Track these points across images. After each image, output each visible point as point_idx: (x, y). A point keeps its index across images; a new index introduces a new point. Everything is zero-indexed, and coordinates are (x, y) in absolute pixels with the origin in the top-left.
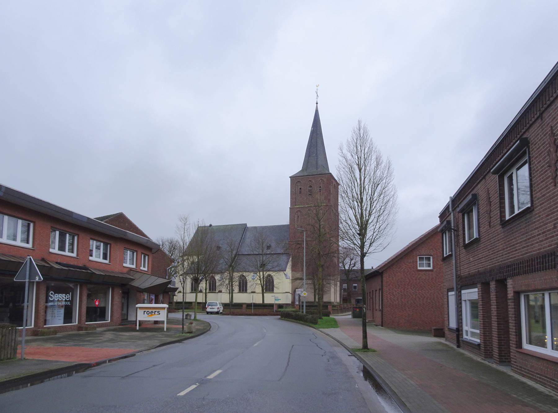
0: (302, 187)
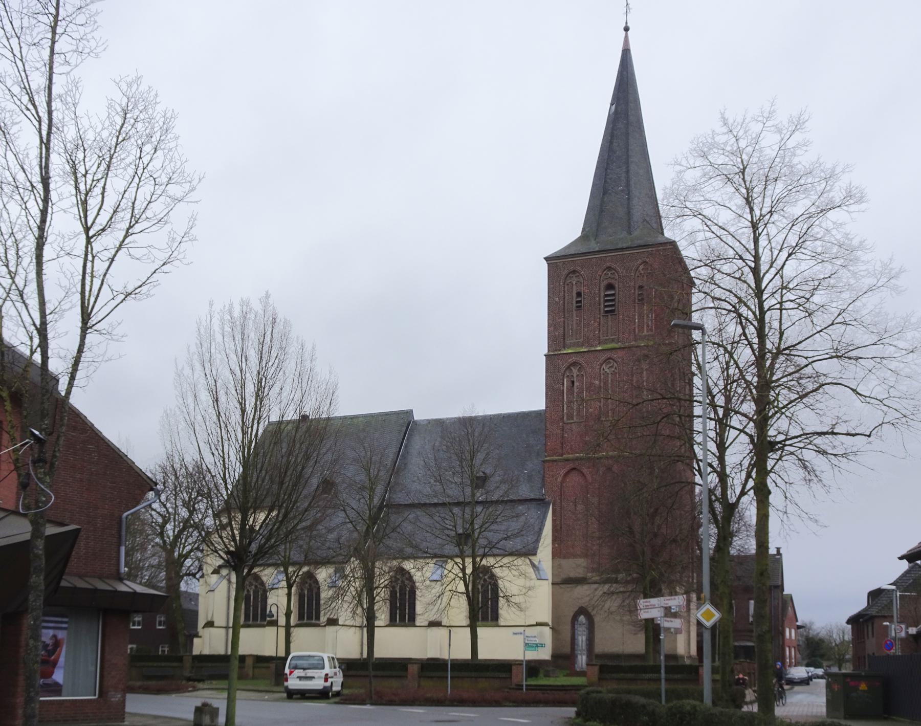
0: (583, 289)
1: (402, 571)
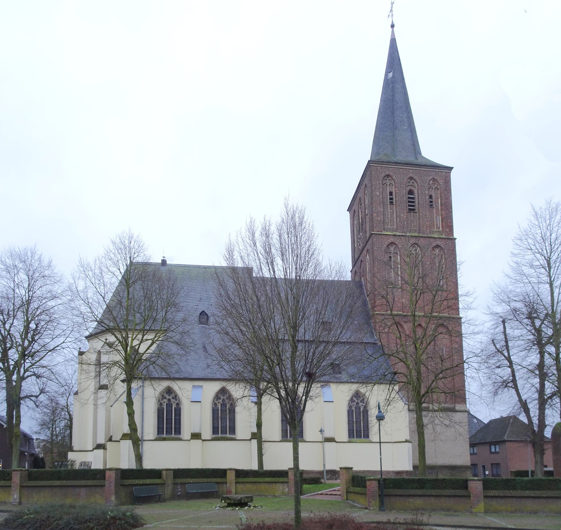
1: (169, 391)
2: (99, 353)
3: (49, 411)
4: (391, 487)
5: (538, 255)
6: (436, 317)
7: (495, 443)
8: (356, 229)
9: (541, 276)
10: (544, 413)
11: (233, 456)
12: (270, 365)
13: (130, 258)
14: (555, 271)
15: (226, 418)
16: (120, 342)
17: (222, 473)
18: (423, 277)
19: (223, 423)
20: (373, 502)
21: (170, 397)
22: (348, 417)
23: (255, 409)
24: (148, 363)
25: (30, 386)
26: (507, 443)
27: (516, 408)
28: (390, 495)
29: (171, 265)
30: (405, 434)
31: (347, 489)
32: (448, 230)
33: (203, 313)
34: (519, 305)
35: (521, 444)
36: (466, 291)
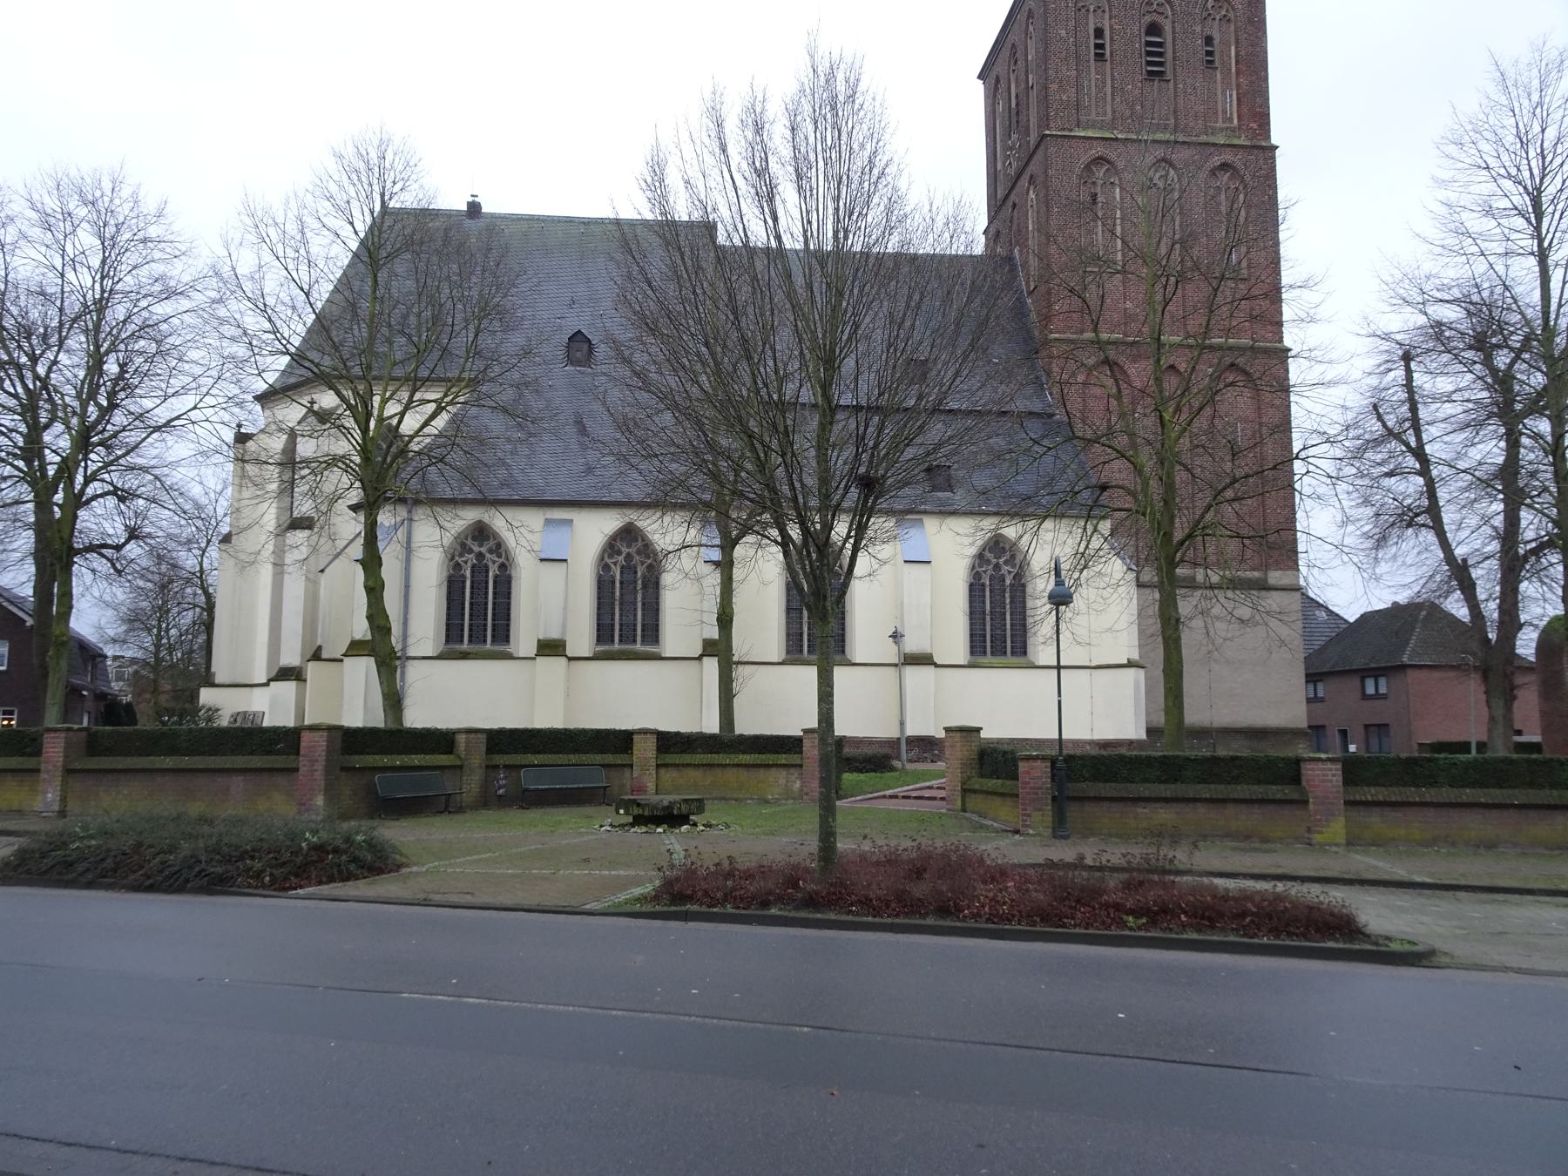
1: (481, 532)
2: (293, 435)
3: (150, 585)
4: (1082, 777)
5: (1508, 185)
6: (1219, 348)
7: (1376, 673)
8: (1002, 124)
9: (1514, 236)
10: (1516, 590)
11: (652, 697)
12: (758, 458)
13: (382, 195)
14: (1555, 223)
15: (635, 603)
16: (349, 407)
17: (620, 742)
18: (1185, 243)
19: (627, 612)
20: (1037, 816)
21: (483, 550)
22: (971, 602)
23: (714, 579)
24: (426, 462)
25: (100, 519)
26: (1409, 671)
27: (1438, 578)
28: (1081, 799)
29: (493, 216)
30: (1125, 645)
31: (963, 783)
32: (1255, 126)
33: (579, 337)
34: (1451, 314)
35: (1452, 674)
36: (1305, 276)
